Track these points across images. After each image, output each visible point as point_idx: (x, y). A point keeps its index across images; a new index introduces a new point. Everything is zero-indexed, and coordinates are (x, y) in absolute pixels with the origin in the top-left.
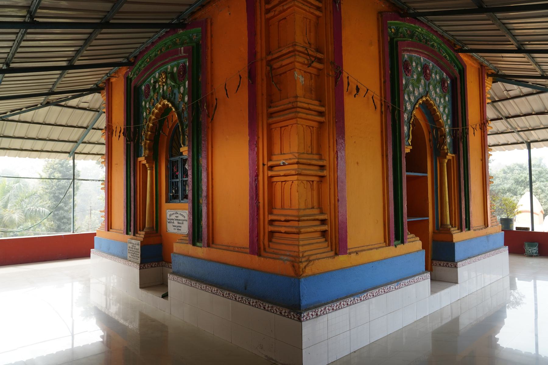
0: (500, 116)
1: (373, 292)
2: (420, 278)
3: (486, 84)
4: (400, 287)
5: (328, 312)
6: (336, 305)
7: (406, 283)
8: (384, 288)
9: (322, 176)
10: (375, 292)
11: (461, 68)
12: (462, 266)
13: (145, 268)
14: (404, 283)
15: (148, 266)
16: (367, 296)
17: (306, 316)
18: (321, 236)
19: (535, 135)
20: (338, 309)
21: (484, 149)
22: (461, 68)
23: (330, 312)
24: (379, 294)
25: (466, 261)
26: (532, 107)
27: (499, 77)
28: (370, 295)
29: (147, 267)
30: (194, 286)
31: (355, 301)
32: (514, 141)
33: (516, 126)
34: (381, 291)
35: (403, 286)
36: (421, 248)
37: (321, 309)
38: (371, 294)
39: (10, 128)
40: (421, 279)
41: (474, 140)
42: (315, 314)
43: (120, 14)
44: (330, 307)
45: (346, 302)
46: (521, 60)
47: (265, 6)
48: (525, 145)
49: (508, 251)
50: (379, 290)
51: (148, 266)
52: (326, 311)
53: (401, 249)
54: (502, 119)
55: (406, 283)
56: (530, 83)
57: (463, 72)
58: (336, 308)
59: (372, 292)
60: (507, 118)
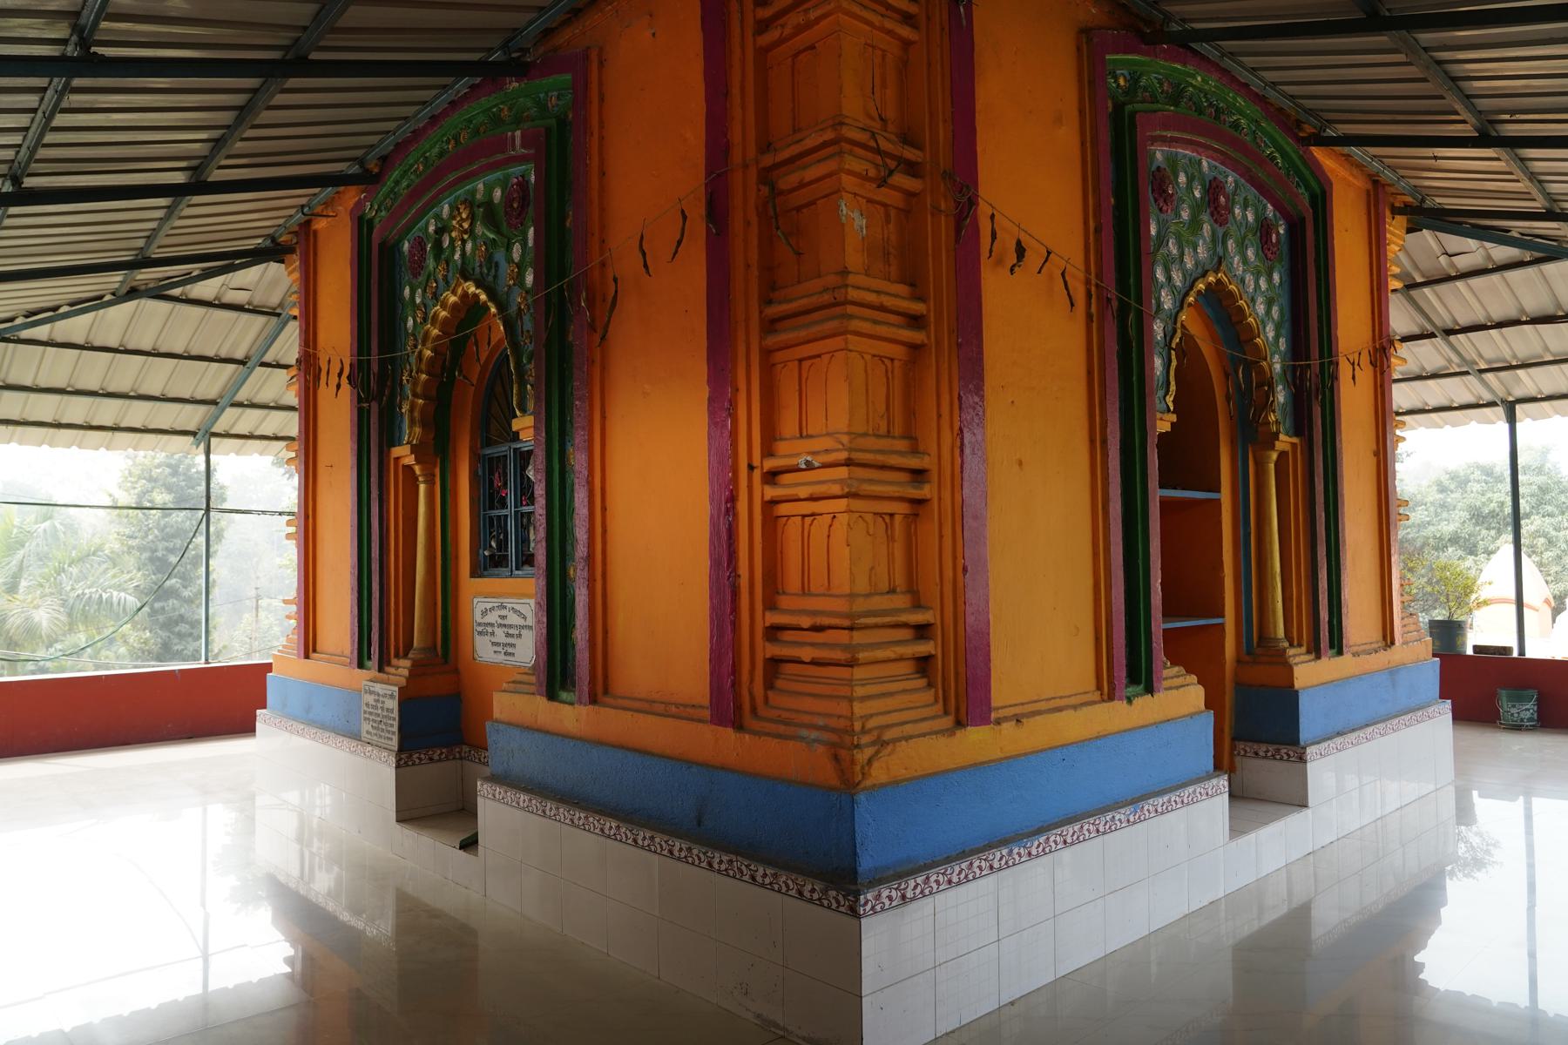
0: (1430, 328)
3: (1388, 236)
4: (1142, 818)
6: (957, 869)
7: (1160, 805)
8: (900, 884)
11: (1318, 191)
12: (1365, 740)
13: (413, 764)
15: (420, 759)
16: (1080, 832)
19: (1528, 382)
20: (965, 880)
21: (1384, 420)
22: (1318, 191)
23: (940, 889)
29: (417, 761)
33: (1474, 355)
34: (1088, 830)
37: (1001, 853)
38: (1058, 838)
40: (1090, 833)
42: (899, 894)
44: (940, 875)
45: (988, 861)
48: (1500, 411)
49: (1451, 714)
50: (1113, 817)
51: (420, 759)
52: (883, 903)
53: (1146, 708)
55: (1160, 805)
57: (1321, 202)
59: (1062, 832)
60: (1449, 332)
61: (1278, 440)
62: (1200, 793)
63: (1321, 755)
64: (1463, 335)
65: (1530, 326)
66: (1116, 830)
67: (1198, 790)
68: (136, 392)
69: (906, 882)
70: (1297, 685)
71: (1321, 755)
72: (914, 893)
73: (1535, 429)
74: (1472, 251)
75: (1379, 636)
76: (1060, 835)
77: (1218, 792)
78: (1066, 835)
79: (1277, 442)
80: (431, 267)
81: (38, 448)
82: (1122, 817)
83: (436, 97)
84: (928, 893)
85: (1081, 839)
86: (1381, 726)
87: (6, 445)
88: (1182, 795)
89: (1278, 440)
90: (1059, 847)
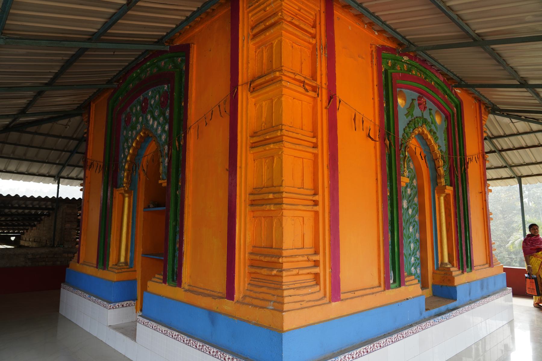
1: (367, 348)
2: (410, 332)
3: (483, 118)
5: (376, 350)
6: (369, 347)
8: (412, 329)
9: (246, 236)
10: (355, 354)
11: (458, 102)
14: (438, 319)
16: (386, 342)
17: (343, 359)
18: (314, 279)
19: (524, 171)
21: (484, 182)
22: (458, 102)
23: (364, 354)
24: (374, 350)
25: (457, 310)
26: (513, 145)
27: (494, 110)
28: (377, 346)
30: (176, 338)
31: (375, 348)
32: (520, 168)
34: (389, 341)
35: (421, 330)
36: (456, 278)
37: (356, 352)
38: (378, 345)
39: (8, 149)
40: (377, 347)
41: (473, 170)
43: (20, 93)
44: (378, 344)
45: (379, 344)
46: (124, 244)
47: (316, 32)
48: (516, 180)
49: (512, 293)
52: (361, 354)
53: (394, 294)
54: (496, 152)
55: (423, 326)
56: (523, 117)
57: (460, 106)
58: (356, 356)
59: (366, 348)
60: (500, 151)
61: (446, 189)
62: (410, 332)
63: (466, 310)
64: (504, 152)
65: (516, 150)
66: (443, 321)
67: (409, 331)
68: (6, 170)
69: (368, 346)
70: (456, 284)
71: (466, 310)
72: (356, 356)
73: (529, 186)
74: (521, 126)
75: (486, 262)
76: (350, 355)
77: (426, 327)
78: (403, 334)
79: (445, 190)
80: (151, 123)
81: (66, 186)
82: (437, 321)
83: (308, 84)
84: (360, 356)
85: (360, 355)
86: (467, 307)
87: (74, 187)
88: (403, 333)
89: (446, 189)
90: (365, 354)
